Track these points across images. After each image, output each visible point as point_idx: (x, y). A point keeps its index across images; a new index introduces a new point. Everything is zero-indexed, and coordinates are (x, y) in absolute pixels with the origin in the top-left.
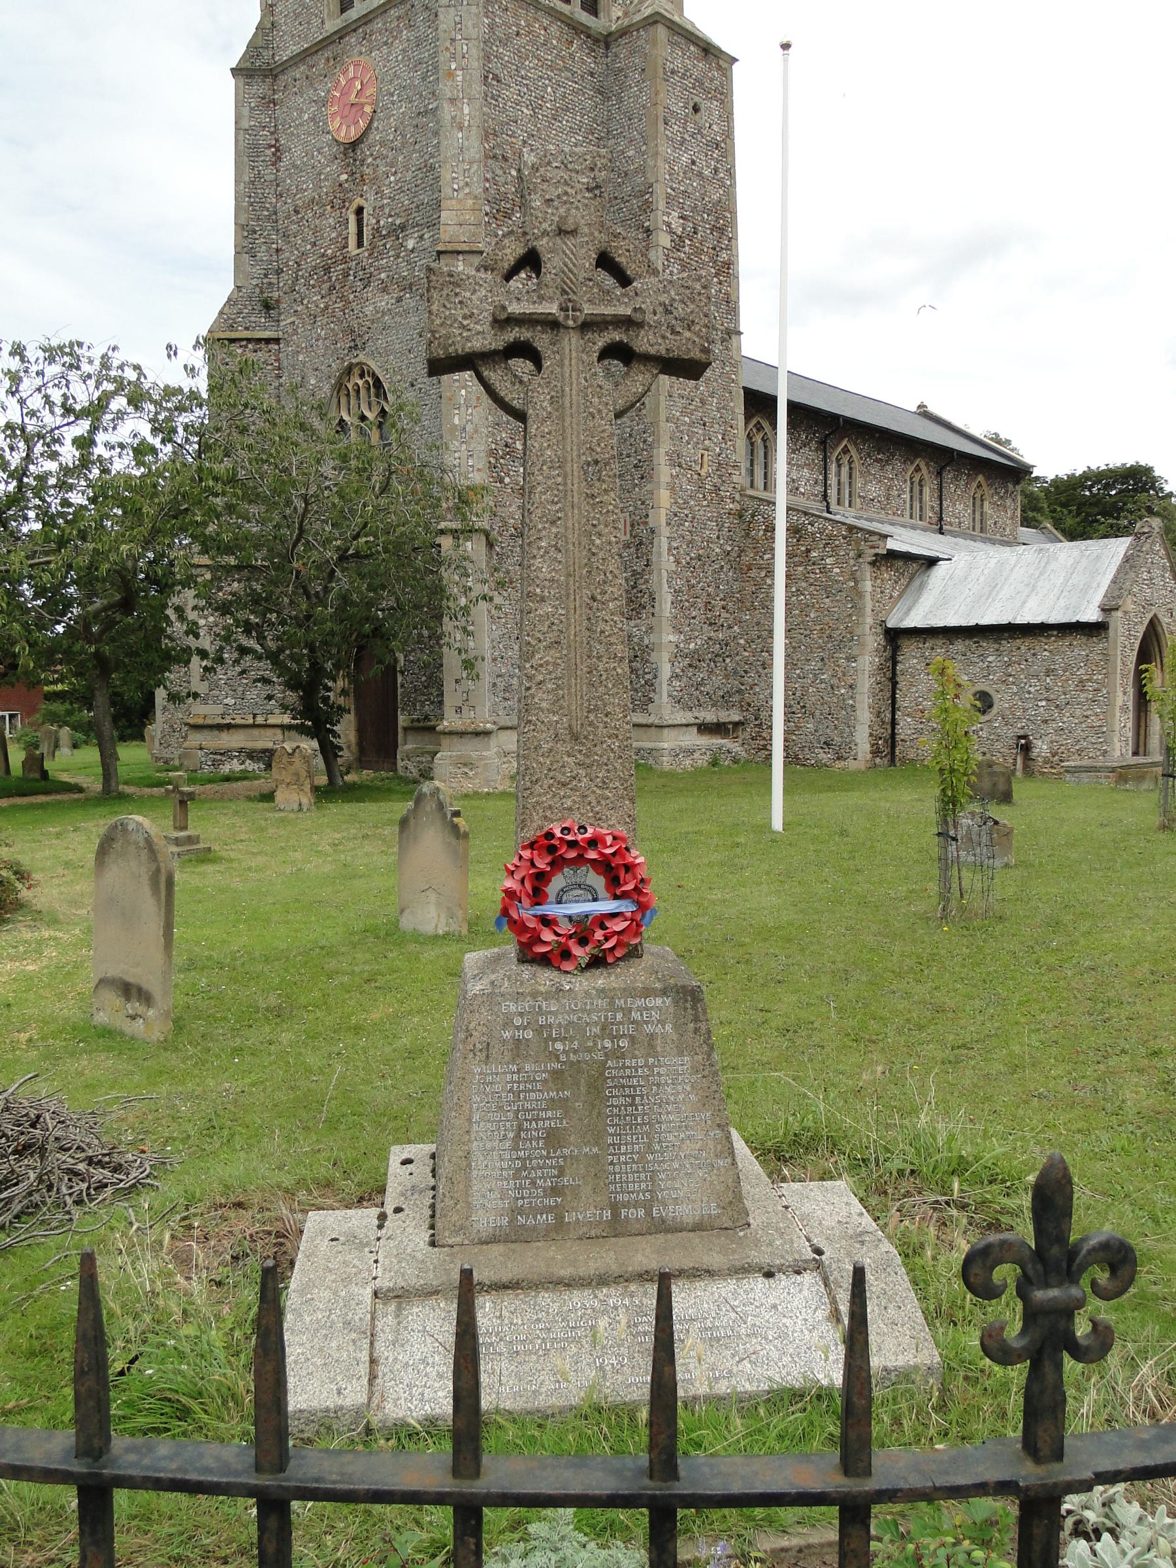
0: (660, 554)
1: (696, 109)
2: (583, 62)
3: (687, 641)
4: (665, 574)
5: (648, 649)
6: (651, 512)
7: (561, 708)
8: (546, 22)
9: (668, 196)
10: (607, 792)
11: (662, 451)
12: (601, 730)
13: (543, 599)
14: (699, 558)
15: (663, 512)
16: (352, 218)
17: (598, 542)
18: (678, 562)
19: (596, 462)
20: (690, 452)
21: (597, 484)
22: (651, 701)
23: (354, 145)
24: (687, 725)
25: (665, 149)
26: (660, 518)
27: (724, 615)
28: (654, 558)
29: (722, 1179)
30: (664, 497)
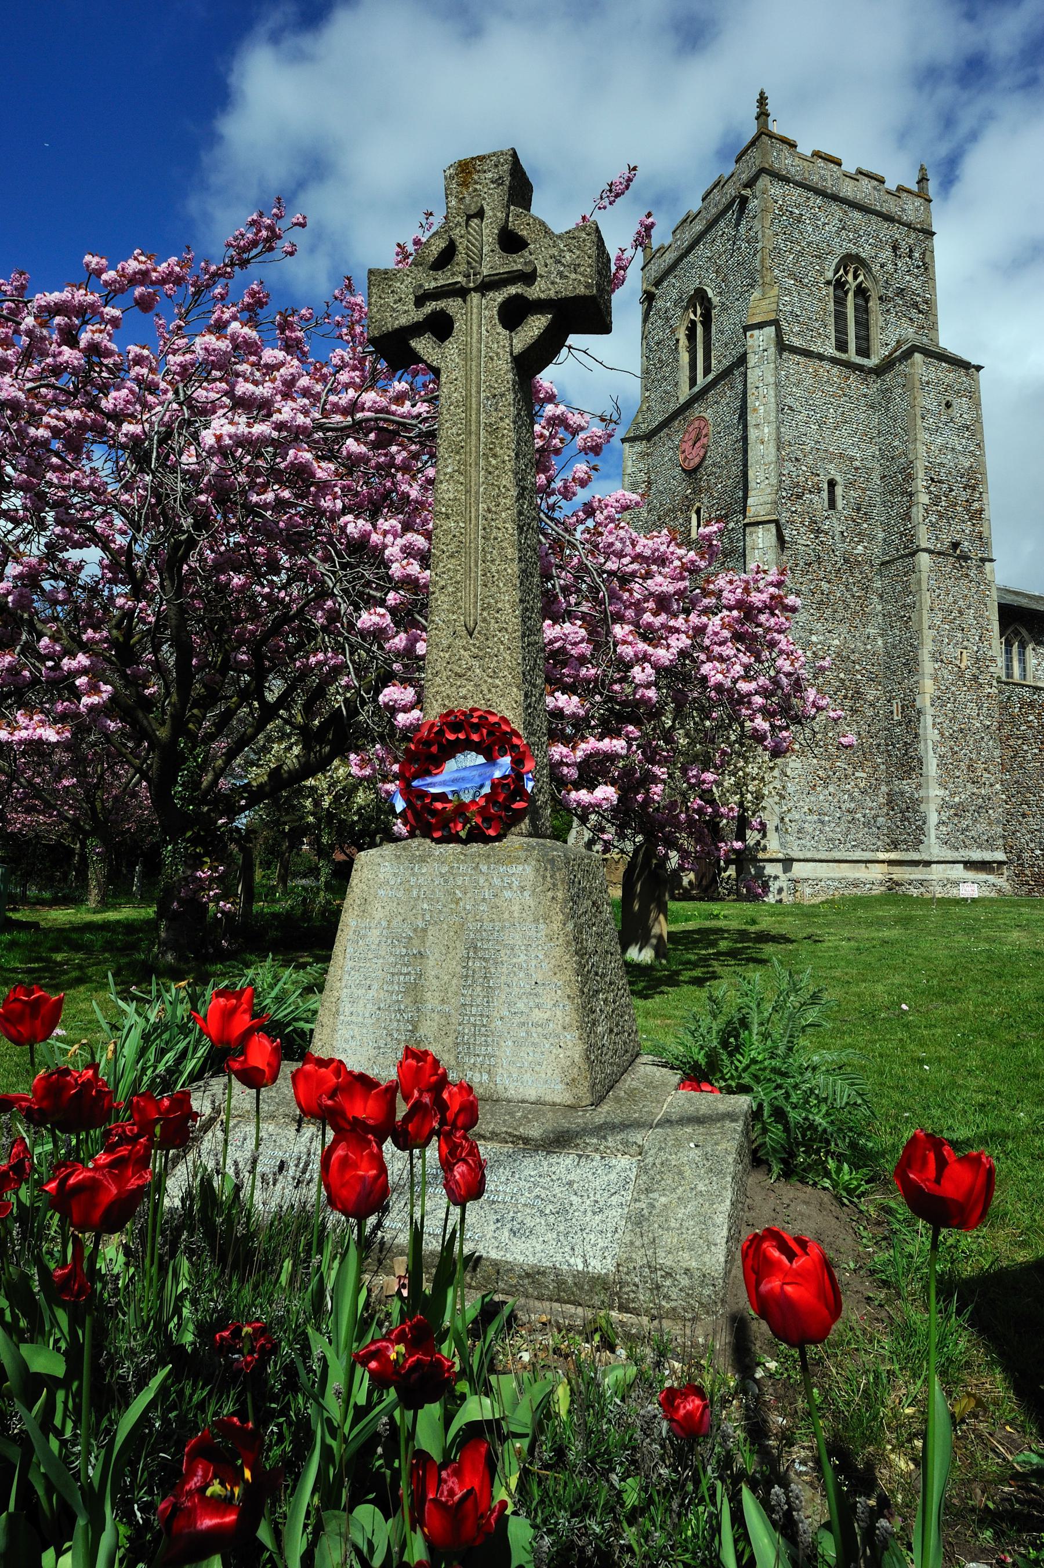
0: (925, 728)
1: (948, 405)
2: (858, 389)
3: (952, 795)
4: (930, 743)
5: (919, 801)
6: (917, 697)
7: (460, 608)
8: (828, 367)
9: (926, 467)
10: (497, 681)
11: (925, 651)
12: (494, 626)
13: (447, 516)
14: (961, 730)
15: (927, 696)
16: (694, 517)
17: (494, 462)
18: (942, 735)
19: (494, 396)
20: (950, 651)
21: (494, 414)
22: (921, 842)
23: (695, 470)
24: (954, 862)
25: (923, 436)
26: (925, 701)
27: (986, 775)
28: (921, 732)
29: (568, 1053)
30: (928, 686)
